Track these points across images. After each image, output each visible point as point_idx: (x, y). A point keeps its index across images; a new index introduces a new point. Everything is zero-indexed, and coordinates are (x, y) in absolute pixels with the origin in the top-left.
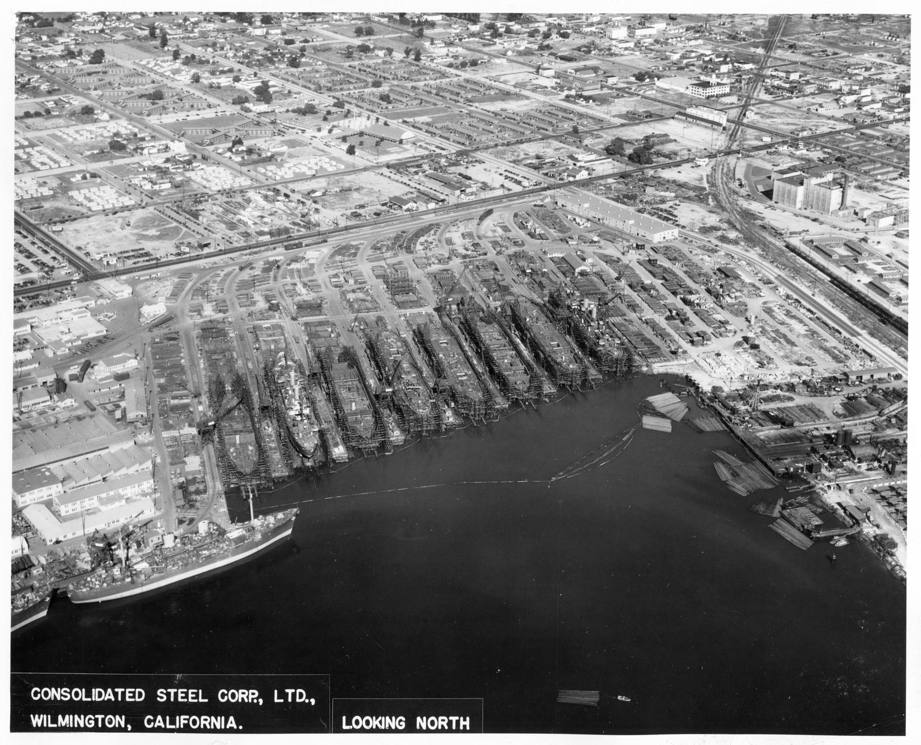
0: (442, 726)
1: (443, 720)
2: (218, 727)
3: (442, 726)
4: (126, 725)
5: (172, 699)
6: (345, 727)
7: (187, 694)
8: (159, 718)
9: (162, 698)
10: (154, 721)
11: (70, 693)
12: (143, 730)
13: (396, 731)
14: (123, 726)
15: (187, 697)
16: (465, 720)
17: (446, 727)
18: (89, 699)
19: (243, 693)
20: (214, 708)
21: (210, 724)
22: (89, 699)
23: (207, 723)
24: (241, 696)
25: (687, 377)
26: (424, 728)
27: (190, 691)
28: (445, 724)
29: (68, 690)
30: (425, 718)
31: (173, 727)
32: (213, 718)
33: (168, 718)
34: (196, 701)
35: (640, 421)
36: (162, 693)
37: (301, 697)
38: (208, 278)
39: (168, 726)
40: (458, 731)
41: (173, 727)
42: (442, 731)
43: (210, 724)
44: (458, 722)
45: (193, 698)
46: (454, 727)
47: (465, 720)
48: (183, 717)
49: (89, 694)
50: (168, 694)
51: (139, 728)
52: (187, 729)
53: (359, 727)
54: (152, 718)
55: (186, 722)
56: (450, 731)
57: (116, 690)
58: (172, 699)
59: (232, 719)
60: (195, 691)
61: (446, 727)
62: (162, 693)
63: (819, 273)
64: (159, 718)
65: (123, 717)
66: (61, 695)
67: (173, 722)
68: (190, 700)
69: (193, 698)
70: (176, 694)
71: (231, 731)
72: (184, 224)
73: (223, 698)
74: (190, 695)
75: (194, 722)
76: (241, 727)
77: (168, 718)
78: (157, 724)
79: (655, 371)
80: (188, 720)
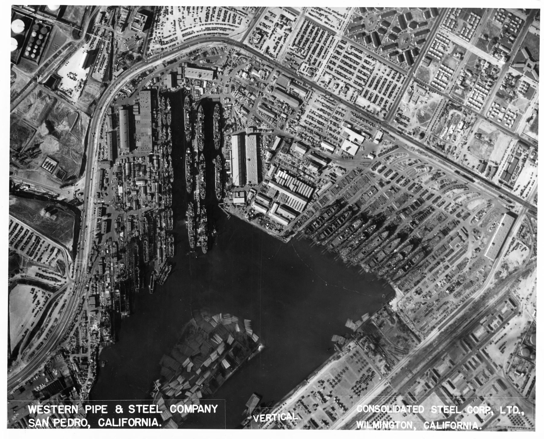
0: (137, 424)
2: (147, 425)
4: (413, 427)
5: (139, 412)
7: (149, 407)
8: (108, 420)
9: (132, 411)
10: (105, 422)
11: (380, 408)
12: (98, 427)
14: (411, 428)
15: (148, 410)
19: (482, 408)
20: (111, 414)
21: (141, 423)
23: (139, 422)
24: (481, 410)
25: (404, 194)
27: (151, 406)
31: (117, 426)
32: (143, 419)
33: (113, 419)
34: (148, 412)
36: (132, 407)
37: (516, 411)
38: (60, 49)
39: (114, 425)
41: (117, 426)
43: (141, 423)
48: (123, 419)
50: (136, 408)
51: (95, 426)
52: (126, 426)
54: (103, 420)
55: (126, 422)
57: (137, 406)
58: (139, 412)
59: (155, 419)
60: (148, 406)
62: (132, 407)
63: (83, 140)
64: (108, 420)
65: (412, 422)
67: (117, 422)
68: (151, 412)
70: (142, 408)
71: (155, 427)
74: (151, 409)
75: (404, 425)
76: (160, 425)
77: (113, 419)
78: (107, 424)
80: (127, 421)
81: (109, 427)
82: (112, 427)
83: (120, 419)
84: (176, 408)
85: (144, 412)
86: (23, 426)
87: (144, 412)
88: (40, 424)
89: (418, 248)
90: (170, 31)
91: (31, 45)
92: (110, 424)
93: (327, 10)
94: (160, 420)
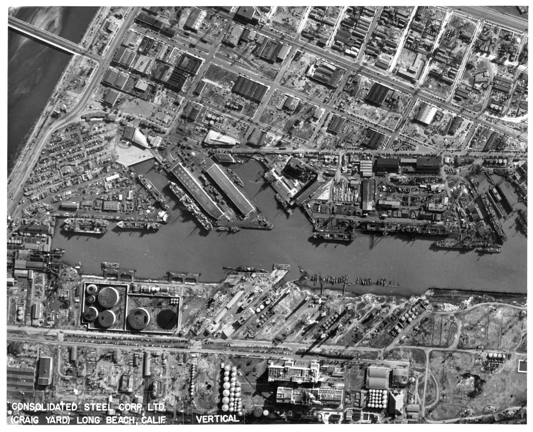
0: (210, 421)
1: (211, 417)
3: (210, 421)
6: (78, 423)
8: (150, 417)
11: (35, 406)
13: (95, 424)
15: (71, 408)
16: (132, 418)
17: (213, 421)
18: (46, 410)
22: (46, 410)
26: (93, 422)
28: (212, 419)
29: (34, 404)
30: (93, 417)
33: (154, 417)
34: (100, 410)
35: (345, 384)
39: (154, 423)
40: (220, 423)
41: (157, 423)
42: (211, 423)
44: (219, 418)
45: (105, 408)
46: (217, 421)
47: (132, 418)
48: (162, 417)
49: (45, 407)
50: (91, 407)
53: (86, 423)
56: (215, 423)
61: (213, 421)
64: (150, 417)
66: (30, 407)
68: (103, 410)
69: (105, 408)
72: (29, 357)
73: (15, 408)
74: (103, 407)
77: (154, 417)
79: (259, 376)
81: (149, 424)
82: (153, 424)
83: (159, 417)
84: (124, 407)
85: (97, 410)
86: (337, 419)
87: (97, 410)
88: (54, 422)
89: (15, 56)
90: (327, 93)
91: (152, 16)
92: (232, 420)
93: (370, 9)
94: (238, 417)
